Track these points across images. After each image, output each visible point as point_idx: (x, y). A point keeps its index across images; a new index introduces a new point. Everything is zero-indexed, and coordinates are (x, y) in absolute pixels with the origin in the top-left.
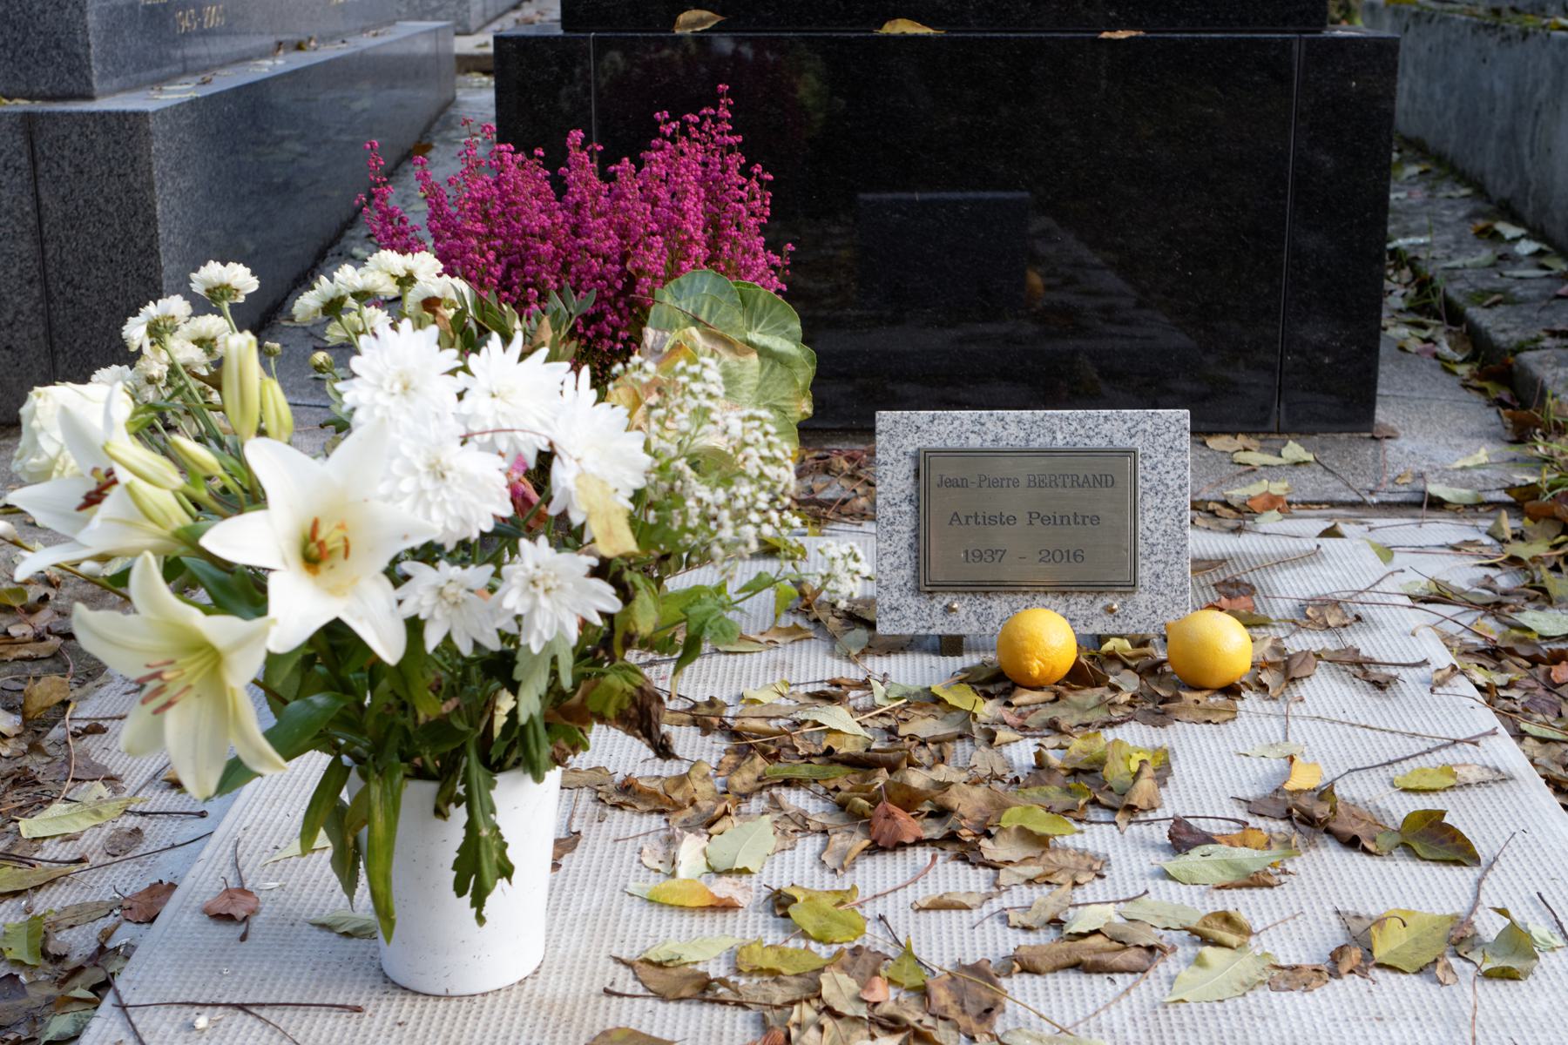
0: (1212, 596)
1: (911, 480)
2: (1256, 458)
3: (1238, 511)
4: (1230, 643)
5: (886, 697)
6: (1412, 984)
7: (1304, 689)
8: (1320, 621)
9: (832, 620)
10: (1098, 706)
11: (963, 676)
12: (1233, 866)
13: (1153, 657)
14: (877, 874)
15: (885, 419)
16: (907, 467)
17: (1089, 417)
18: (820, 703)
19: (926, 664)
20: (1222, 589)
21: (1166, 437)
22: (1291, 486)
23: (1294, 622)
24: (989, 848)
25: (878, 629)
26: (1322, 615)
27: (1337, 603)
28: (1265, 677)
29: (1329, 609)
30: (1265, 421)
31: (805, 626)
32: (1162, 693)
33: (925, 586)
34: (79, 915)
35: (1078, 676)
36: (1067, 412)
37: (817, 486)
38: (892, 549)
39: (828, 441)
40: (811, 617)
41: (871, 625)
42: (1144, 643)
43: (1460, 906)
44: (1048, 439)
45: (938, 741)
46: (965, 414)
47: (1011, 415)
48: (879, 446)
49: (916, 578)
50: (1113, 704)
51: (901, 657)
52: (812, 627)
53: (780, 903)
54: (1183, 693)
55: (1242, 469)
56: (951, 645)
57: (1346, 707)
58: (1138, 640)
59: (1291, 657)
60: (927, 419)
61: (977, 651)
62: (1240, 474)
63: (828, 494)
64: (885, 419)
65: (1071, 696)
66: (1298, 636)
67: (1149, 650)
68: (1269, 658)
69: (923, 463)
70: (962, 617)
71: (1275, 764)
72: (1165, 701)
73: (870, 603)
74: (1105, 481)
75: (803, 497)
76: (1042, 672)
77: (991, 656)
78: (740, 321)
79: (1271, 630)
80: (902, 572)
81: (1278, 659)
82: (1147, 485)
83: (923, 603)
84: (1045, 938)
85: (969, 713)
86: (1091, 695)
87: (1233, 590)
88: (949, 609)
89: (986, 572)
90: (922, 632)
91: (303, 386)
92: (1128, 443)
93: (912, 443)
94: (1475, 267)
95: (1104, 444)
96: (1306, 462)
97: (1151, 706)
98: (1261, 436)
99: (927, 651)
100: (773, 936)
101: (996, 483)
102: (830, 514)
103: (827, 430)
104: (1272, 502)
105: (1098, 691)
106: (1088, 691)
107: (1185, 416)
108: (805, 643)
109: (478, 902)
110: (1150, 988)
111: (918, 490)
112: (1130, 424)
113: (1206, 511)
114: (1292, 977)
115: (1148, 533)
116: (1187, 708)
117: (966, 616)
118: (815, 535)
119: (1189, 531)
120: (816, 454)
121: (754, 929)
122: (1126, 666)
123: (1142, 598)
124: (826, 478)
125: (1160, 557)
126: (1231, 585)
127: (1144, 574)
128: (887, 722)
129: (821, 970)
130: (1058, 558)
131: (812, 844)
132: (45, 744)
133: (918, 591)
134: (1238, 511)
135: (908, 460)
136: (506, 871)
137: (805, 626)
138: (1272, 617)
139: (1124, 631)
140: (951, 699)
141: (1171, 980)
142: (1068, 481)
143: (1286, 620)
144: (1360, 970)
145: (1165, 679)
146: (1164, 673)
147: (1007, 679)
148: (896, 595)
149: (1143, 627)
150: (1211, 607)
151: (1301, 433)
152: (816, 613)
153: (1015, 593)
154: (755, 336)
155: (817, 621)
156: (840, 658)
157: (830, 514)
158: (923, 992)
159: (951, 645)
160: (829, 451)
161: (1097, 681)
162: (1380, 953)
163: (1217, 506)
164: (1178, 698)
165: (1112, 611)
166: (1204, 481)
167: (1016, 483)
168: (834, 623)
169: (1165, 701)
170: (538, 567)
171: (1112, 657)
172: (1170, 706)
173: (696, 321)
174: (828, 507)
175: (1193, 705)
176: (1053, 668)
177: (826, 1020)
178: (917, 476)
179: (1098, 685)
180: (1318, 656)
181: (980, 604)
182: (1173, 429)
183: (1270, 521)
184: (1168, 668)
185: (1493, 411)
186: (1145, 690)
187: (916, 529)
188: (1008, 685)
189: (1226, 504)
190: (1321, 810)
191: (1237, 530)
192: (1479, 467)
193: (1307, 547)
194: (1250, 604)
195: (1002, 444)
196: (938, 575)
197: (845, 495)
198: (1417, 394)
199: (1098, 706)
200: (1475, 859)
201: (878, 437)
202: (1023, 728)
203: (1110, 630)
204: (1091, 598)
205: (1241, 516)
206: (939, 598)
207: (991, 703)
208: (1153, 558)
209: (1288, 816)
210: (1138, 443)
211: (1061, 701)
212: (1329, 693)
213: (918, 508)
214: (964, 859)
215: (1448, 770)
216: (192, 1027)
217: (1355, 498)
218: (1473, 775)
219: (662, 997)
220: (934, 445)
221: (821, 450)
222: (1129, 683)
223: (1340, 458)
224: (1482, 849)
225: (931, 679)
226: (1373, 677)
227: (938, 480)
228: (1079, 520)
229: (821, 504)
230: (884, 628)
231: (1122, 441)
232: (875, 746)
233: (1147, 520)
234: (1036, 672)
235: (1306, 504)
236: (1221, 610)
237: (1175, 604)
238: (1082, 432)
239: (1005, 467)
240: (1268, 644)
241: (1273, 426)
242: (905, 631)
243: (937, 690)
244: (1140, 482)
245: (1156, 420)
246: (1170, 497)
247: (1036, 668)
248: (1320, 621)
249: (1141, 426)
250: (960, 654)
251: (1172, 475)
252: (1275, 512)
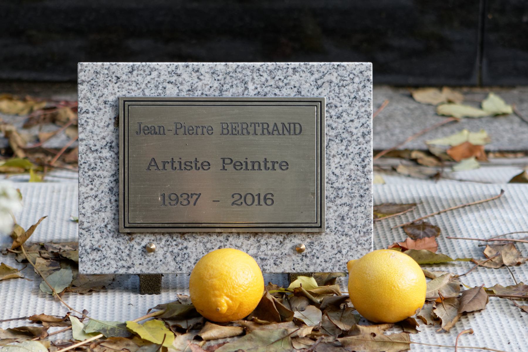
0: (399, 237)
1: (112, 127)
2: (459, 110)
3: (438, 159)
4: (405, 281)
5: (84, 333)
7: (475, 323)
8: (496, 260)
9: (40, 260)
10: (282, 339)
11: (158, 312)
13: (338, 293)
15: (87, 69)
16: (107, 115)
17: (278, 69)
18: (20, 338)
19: (125, 302)
20: (410, 231)
21: (350, 87)
22: (490, 137)
23: (472, 261)
25: (80, 269)
26: (498, 255)
27: (513, 244)
28: (439, 312)
29: (506, 248)
30: (467, 76)
31: (14, 266)
32: (342, 327)
33: (126, 226)
35: (265, 312)
36: (258, 64)
37: (44, 135)
38: (93, 193)
39: (57, 92)
40: (20, 259)
41: (75, 265)
42: (331, 281)
44: (240, 90)
46: (162, 66)
47: (205, 66)
48: (81, 95)
49: (116, 220)
50: (296, 338)
51: (102, 295)
52: (20, 267)
54: (361, 327)
55: (445, 120)
56: (150, 284)
57: (511, 338)
58: (326, 277)
59: (465, 293)
60: (126, 70)
61: (175, 289)
62: (443, 125)
63: (54, 143)
64: (87, 69)
65: (258, 331)
66: (475, 274)
67: (335, 287)
68: (445, 295)
69: (124, 112)
70: (160, 257)
72: (344, 334)
73: (75, 245)
74: (292, 129)
75: (30, 145)
76: (230, 308)
77: (187, 294)
79: (451, 269)
80: (103, 215)
81: (454, 295)
82: (333, 133)
83: (122, 243)
85: (159, 346)
86: (276, 329)
87: (419, 235)
88: (147, 250)
90: (122, 271)
92: (315, 94)
93: (113, 92)
95: (292, 94)
96: (504, 114)
97: (331, 339)
98: (465, 90)
99: (127, 289)
101: (190, 131)
102: (55, 162)
103: (19, 81)
104: (471, 151)
105: (283, 326)
106: (274, 326)
107: (368, 69)
108: (12, 282)
111: (117, 138)
112: (316, 76)
113: (391, 158)
115: (334, 178)
116: (364, 341)
117: (163, 256)
118: (37, 181)
119: (372, 176)
120: (45, 105)
122: (311, 303)
123: (328, 238)
124: (52, 128)
125: (345, 200)
126: (418, 227)
127: (330, 216)
130: (249, 202)
133: (118, 233)
134: (438, 159)
135: (108, 109)
137: (14, 266)
138: (453, 257)
139: (311, 269)
140: (144, 334)
142: (259, 129)
143: (465, 259)
145: (346, 314)
146: (346, 309)
147: (198, 315)
148: (97, 236)
149: (329, 265)
150: (397, 247)
151: (502, 86)
152: (25, 254)
153: (209, 234)
155: (25, 262)
156: (43, 296)
157: (55, 162)
159: (150, 284)
160: (58, 102)
161: (282, 316)
163: (421, 155)
164: (356, 331)
165: (300, 251)
166: (409, 132)
167: (210, 131)
168: (40, 264)
169: (344, 334)
170: (346, 274)
171: (299, 294)
172: (348, 339)
174: (53, 155)
175: (369, 337)
176: (241, 304)
178: (117, 124)
179: (283, 320)
180: (490, 292)
181: (176, 244)
182: (357, 80)
183: (467, 169)
184: (350, 305)
186: (327, 324)
187: (116, 174)
188: (200, 320)
189: (428, 153)
191: (436, 177)
193: (492, 192)
194: (434, 245)
195: (197, 94)
197: (70, 144)
199: (282, 339)
201: (80, 87)
203: (299, 269)
204: (280, 238)
205: (440, 163)
206: (138, 239)
207: (181, 338)
208: (339, 201)
210: (324, 93)
211: (248, 336)
212: (497, 326)
213: (117, 154)
220: (133, 94)
221: (49, 100)
222: (312, 318)
225: (129, 317)
227: (137, 127)
228: (269, 165)
229: (47, 152)
230: (86, 268)
231: (309, 91)
233: (333, 165)
234: (224, 308)
235: (503, 153)
236: (403, 250)
237: (358, 244)
238: (272, 82)
239: (214, 118)
240: (446, 281)
241: (475, 79)
242: (105, 271)
243: (132, 326)
244: (326, 130)
245: (341, 72)
246: (354, 144)
247: (224, 304)
248: (496, 260)
249: (327, 78)
250: (158, 292)
251: (356, 123)
252: (472, 160)
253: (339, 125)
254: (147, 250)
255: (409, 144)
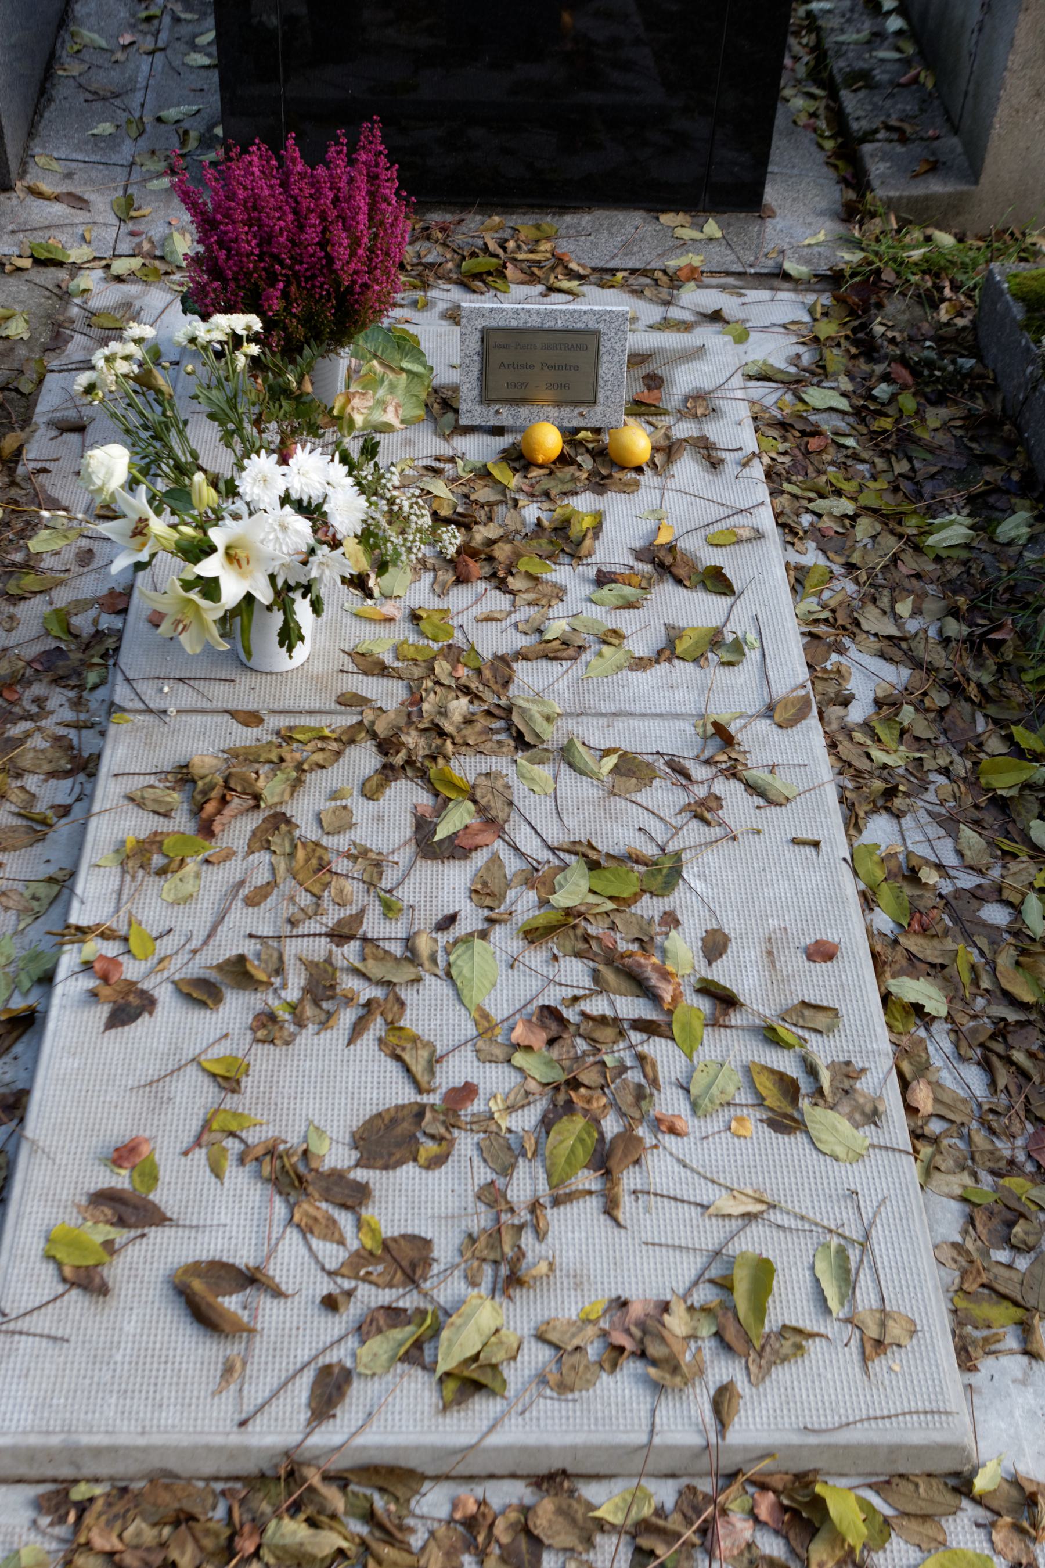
2: (688, 233)
6: (690, 667)
12: (623, 597)
14: (460, 598)
24: (513, 583)
34: (82, 605)
35: (563, 459)
43: (716, 622)
45: (491, 505)
53: (415, 617)
63: (430, 259)
71: (652, 524)
72: (604, 478)
74: (583, 347)
78: (398, 357)
84: (534, 638)
88: (497, 412)
89: (519, 394)
91: (86, 143)
94: (856, 43)
100: (413, 638)
109: (290, 650)
110: (577, 669)
114: (640, 664)
117: (506, 416)
121: (403, 631)
123: (599, 409)
124: (427, 244)
127: (601, 396)
128: (465, 490)
129: (434, 658)
131: (427, 577)
132: (18, 479)
133: (481, 402)
136: (302, 638)
141: (587, 664)
144: (669, 660)
154: (405, 365)
158: (479, 672)
159: (498, 431)
162: (679, 651)
169: (604, 478)
173: (375, 356)
177: (438, 689)
181: (514, 409)
185: (838, 187)
190: (668, 560)
192: (818, 244)
196: (491, 395)
197: (440, 260)
198: (795, 171)
200: (733, 592)
202: (533, 495)
203: (582, 424)
209: (653, 562)
210: (601, 326)
214: (498, 588)
215: (731, 531)
216: (161, 690)
217: (741, 269)
218: (745, 533)
219: (365, 673)
223: (738, 234)
224: (737, 586)
226: (710, 456)
232: (460, 510)
253: (608, 345)
254: (497, 412)
255: (654, 265)
